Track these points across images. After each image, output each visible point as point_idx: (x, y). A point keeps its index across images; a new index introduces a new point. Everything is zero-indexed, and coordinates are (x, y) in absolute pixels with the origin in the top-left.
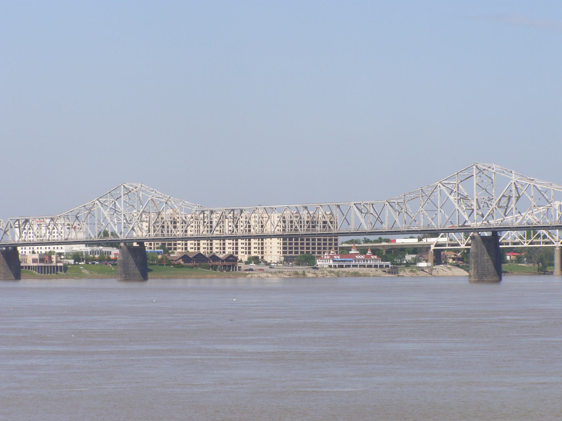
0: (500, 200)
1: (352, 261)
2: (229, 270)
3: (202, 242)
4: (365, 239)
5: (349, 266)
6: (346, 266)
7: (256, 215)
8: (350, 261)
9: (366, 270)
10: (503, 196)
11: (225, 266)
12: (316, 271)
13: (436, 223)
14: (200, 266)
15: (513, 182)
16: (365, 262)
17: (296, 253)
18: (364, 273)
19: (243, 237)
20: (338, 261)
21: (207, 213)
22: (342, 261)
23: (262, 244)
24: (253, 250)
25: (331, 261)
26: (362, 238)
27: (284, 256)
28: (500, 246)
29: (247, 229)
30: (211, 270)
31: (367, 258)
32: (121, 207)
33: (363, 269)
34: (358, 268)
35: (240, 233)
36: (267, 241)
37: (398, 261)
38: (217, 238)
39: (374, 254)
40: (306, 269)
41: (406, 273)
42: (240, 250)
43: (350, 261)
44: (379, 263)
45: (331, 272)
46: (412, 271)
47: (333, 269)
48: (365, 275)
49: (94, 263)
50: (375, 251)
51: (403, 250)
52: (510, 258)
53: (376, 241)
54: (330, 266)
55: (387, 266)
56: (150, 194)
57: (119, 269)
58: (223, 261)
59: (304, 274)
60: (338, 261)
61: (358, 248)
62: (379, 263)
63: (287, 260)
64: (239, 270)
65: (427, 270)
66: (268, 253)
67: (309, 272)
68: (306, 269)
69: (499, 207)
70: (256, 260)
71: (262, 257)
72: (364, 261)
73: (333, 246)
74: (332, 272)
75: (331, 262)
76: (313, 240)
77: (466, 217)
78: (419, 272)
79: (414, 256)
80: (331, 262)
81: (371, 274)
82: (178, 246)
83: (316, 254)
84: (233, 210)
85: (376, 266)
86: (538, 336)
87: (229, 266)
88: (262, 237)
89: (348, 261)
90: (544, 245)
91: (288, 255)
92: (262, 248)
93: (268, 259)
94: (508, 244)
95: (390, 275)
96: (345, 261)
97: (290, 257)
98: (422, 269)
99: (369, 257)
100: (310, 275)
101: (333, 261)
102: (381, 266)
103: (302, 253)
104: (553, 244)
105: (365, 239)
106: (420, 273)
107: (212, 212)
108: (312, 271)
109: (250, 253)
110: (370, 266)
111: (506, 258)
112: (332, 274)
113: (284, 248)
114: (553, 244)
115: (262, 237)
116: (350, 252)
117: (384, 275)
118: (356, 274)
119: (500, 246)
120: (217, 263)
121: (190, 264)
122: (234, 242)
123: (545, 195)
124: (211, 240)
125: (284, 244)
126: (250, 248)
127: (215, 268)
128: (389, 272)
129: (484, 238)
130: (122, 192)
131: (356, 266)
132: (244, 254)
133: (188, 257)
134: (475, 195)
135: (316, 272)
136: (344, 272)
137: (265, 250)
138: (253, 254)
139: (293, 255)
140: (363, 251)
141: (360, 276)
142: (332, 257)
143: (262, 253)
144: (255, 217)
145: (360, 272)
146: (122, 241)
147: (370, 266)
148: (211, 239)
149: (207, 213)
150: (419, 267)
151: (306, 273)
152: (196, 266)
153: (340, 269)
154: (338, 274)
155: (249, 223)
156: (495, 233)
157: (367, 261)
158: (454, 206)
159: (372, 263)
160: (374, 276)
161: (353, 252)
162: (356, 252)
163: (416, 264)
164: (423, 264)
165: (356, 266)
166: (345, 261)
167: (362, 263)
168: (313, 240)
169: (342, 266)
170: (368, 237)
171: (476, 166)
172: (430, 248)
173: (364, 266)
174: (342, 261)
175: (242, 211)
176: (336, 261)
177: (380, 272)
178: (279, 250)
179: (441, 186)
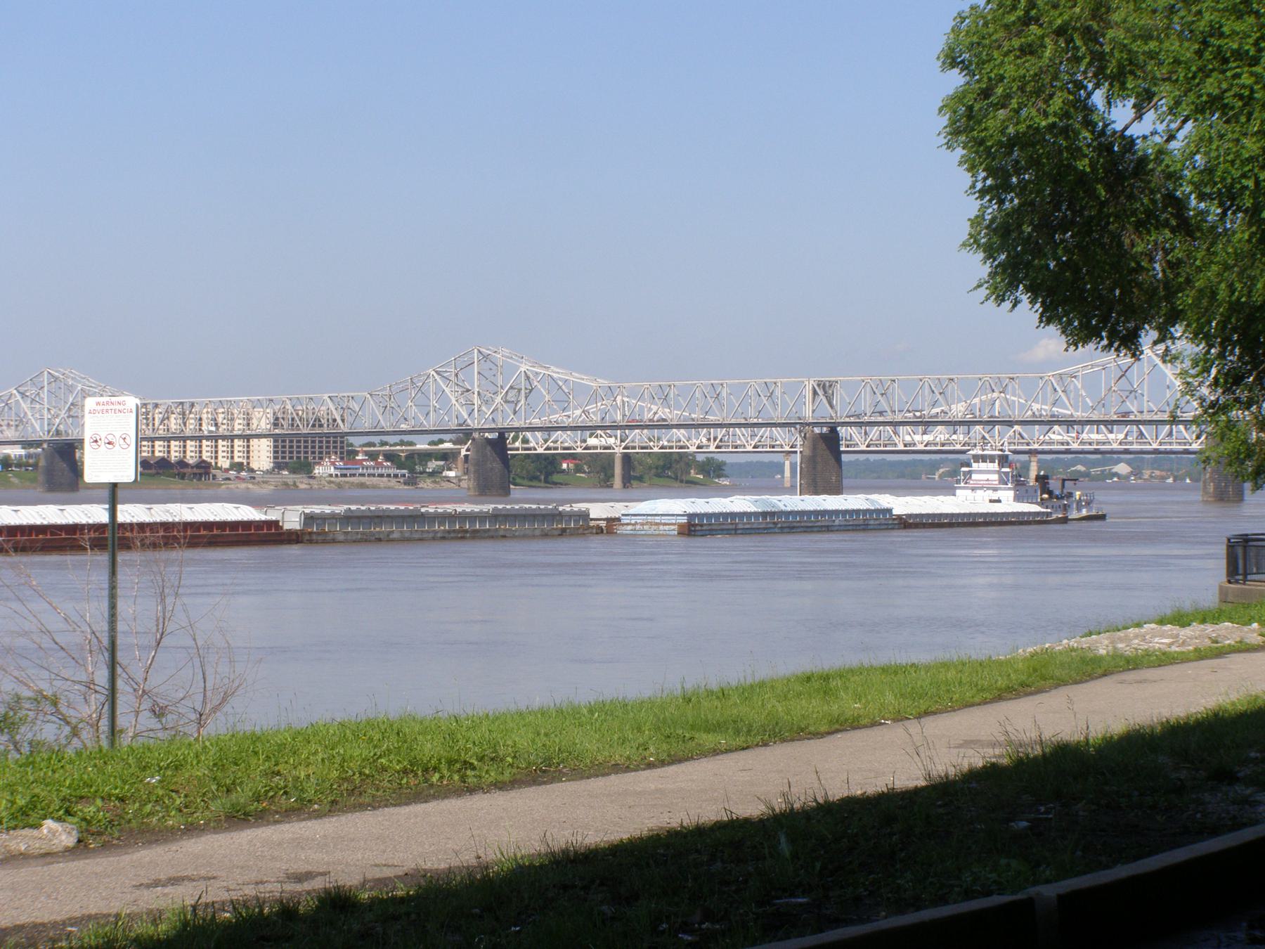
0: (507, 392)
1: (359, 469)
2: (200, 479)
3: (157, 443)
4: (381, 441)
5: (354, 475)
6: (351, 475)
7: (209, 410)
8: (356, 469)
9: (375, 480)
10: (511, 387)
11: (195, 474)
12: (312, 481)
13: (428, 422)
14: (163, 474)
15: (523, 370)
16: (365, 471)
17: (284, 458)
18: (373, 485)
19: (192, 438)
20: (341, 469)
21: (150, 407)
22: (347, 469)
23: (248, 446)
24: (236, 454)
25: (332, 468)
26: (376, 439)
27: (274, 463)
28: (509, 452)
29: (197, 427)
30: (177, 479)
31: (379, 465)
32: (165, 403)
33: (372, 478)
34: (367, 478)
35: (188, 433)
36: (254, 442)
37: (418, 468)
38: (224, 438)
39: (386, 461)
40: (298, 478)
41: (426, 484)
42: (220, 454)
43: (356, 469)
44: (393, 471)
45: (330, 482)
46: (435, 482)
47: (332, 479)
48: (375, 487)
49: (27, 470)
50: (390, 457)
51: (426, 456)
52: (568, 466)
53: (396, 444)
54: (331, 475)
55: (404, 476)
56: (80, 382)
57: (41, 478)
58: (192, 467)
59: (295, 484)
60: (341, 469)
61: (366, 453)
62: (393, 471)
63: (278, 466)
64: (213, 479)
65: (454, 481)
66: (256, 458)
67: (302, 483)
68: (298, 478)
69: (506, 402)
70: (239, 467)
71: (248, 463)
72: (374, 469)
73: (338, 450)
74: (332, 482)
75: (332, 471)
76: (299, 441)
77: (466, 416)
78: (443, 484)
79: (442, 463)
80: (332, 471)
81: (382, 485)
82: (144, 449)
83: (317, 460)
84: (182, 403)
85: (389, 476)
86: (196, 594)
87: (201, 475)
88: (248, 438)
89: (353, 469)
90: (602, 451)
91: (280, 460)
92: (248, 452)
93: (254, 465)
94: (634, 448)
95: (406, 487)
96: (349, 469)
97: (283, 463)
98: (448, 480)
99: (381, 463)
100: (302, 486)
101: (335, 468)
102: (396, 476)
103: (298, 458)
104: (614, 449)
105: (381, 441)
106: (445, 485)
107: (156, 406)
108: (306, 481)
109: (232, 457)
110: (381, 476)
111: (562, 465)
112: (332, 485)
113: (276, 452)
114: (614, 449)
115: (248, 438)
116: (357, 458)
117: (398, 486)
118: (362, 485)
119: (509, 452)
120: (185, 470)
121: (150, 471)
122: (182, 443)
123: (563, 387)
124: (153, 442)
125: (275, 447)
126: (232, 452)
127: (183, 476)
128: (405, 483)
129: (488, 440)
130: (46, 380)
131: (363, 475)
132: (225, 459)
133: (148, 463)
134: (476, 386)
135: (311, 483)
136: (347, 482)
137: (251, 454)
138: (237, 460)
139: (287, 460)
140: (372, 456)
141: (368, 488)
142: (333, 464)
143: (248, 458)
144: (208, 412)
145: (368, 483)
146: (45, 441)
147: (381, 476)
148: (153, 440)
149: (150, 407)
150: (446, 477)
151: (298, 484)
152: (158, 473)
153: (343, 479)
154: (339, 486)
155: (215, 420)
156: (502, 434)
157: (378, 468)
158: (451, 400)
159: (383, 471)
160: (385, 488)
161: (360, 457)
162: (364, 458)
163: (442, 473)
164: (452, 474)
165: (363, 475)
166: (349, 469)
167: (371, 471)
168: (291, 441)
169: (345, 475)
170: (385, 438)
171: (479, 350)
172: (460, 453)
173: (374, 475)
174: (347, 469)
175: (192, 405)
176: (338, 469)
177: (393, 482)
178: (268, 454)
179: (435, 374)
